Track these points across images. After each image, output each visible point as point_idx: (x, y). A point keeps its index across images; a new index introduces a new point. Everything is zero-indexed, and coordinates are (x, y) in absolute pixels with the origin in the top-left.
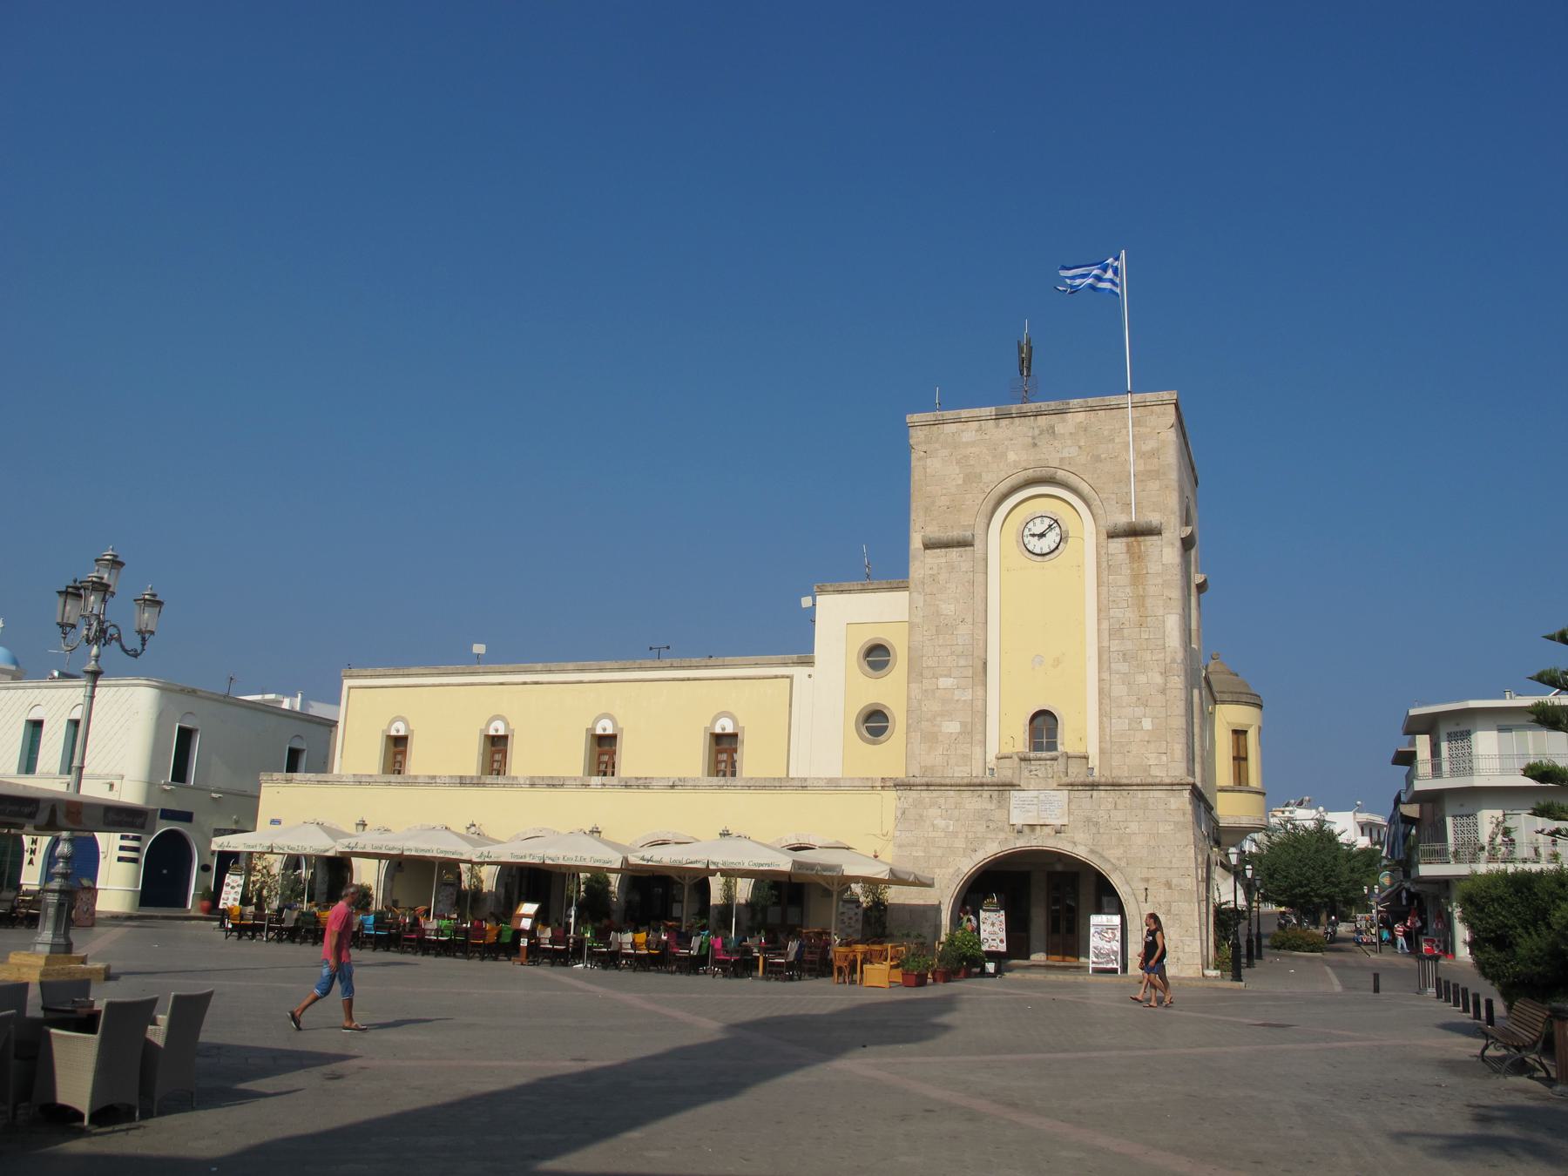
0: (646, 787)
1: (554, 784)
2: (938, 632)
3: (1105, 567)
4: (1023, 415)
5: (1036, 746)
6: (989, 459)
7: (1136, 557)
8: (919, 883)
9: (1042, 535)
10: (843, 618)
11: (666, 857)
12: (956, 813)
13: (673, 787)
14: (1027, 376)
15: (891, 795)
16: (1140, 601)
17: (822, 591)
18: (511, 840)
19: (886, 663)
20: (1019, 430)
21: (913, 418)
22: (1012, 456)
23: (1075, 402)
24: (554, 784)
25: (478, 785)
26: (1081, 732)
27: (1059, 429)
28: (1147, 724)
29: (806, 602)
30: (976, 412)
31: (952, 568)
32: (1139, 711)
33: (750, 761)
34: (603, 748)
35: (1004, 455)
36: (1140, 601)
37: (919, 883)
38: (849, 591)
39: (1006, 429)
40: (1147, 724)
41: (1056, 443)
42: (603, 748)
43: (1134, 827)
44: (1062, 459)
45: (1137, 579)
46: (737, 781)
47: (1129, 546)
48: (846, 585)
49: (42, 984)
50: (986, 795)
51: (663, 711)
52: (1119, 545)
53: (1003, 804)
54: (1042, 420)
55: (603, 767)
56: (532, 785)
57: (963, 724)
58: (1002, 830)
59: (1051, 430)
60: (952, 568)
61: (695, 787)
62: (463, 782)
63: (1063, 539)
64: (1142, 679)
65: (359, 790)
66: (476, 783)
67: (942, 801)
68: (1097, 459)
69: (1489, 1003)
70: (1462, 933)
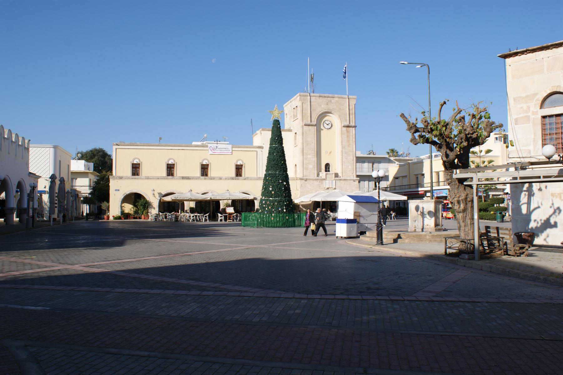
3: (342, 133)
4: (325, 97)
7: (348, 132)
11: (208, 197)
14: (512, 225)
15: (299, 181)
16: (348, 141)
18: (507, 167)
20: (325, 100)
22: (323, 106)
23: (336, 96)
26: (336, 168)
27: (332, 101)
28: (350, 167)
31: (310, 130)
36: (348, 141)
39: (321, 100)
45: (348, 136)
54: (329, 99)
59: (331, 101)
60: (310, 130)
65: (147, 181)
68: (340, 109)
69: (438, 173)
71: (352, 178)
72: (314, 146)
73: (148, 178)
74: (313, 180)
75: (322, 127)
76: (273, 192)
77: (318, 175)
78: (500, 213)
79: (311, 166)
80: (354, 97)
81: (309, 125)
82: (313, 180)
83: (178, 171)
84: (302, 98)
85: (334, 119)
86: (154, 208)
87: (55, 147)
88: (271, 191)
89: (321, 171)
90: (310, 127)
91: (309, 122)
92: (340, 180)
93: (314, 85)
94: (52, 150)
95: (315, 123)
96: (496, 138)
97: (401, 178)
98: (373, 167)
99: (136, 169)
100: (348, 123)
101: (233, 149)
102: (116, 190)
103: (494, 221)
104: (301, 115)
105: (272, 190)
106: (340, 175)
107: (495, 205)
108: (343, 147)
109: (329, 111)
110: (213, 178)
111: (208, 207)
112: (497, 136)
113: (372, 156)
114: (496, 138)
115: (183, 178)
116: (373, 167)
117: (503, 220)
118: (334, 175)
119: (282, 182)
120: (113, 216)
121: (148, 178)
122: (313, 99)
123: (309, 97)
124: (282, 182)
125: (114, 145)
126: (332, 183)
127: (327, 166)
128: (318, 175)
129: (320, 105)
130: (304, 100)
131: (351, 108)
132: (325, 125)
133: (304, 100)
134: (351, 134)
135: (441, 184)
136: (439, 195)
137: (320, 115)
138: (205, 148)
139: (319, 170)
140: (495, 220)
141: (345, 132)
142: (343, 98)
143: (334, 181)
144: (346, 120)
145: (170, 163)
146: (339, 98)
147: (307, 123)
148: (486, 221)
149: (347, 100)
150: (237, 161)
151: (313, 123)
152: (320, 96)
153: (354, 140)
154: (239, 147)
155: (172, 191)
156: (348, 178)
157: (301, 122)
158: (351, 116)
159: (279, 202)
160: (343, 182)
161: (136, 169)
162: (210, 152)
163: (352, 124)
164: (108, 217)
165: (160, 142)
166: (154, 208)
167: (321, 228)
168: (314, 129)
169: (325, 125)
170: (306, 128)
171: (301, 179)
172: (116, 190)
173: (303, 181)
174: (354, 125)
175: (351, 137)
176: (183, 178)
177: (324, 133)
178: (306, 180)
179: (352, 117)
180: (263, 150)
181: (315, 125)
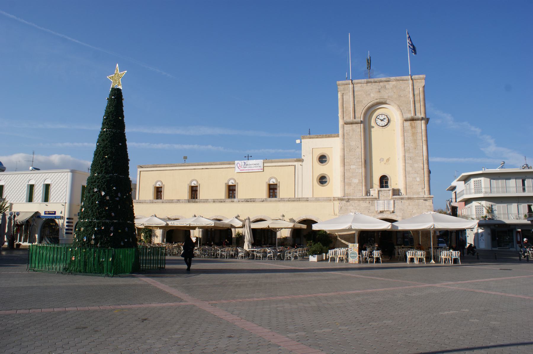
0: (254, 201)
2: (350, 151)
3: (404, 130)
4: (376, 82)
5: (229, 197)
6: (365, 96)
7: (413, 127)
8: (261, 220)
9: (382, 120)
10: (311, 146)
12: (358, 208)
13: (263, 201)
15: (337, 203)
16: (415, 141)
17: (304, 138)
19: (326, 161)
20: (375, 86)
21: (338, 82)
22: (372, 95)
23: (392, 78)
25: (152, 202)
26: (397, 181)
27: (387, 86)
28: (418, 179)
29: (298, 141)
30: (360, 81)
31: (353, 130)
32: (416, 175)
33: (282, 192)
34: (194, 192)
35: (370, 94)
37: (261, 220)
38: (313, 138)
40: (418, 179)
41: (386, 91)
42: (194, 192)
43: (415, 211)
44: (389, 96)
45: (414, 134)
46: (235, 200)
47: (411, 124)
50: (367, 202)
51: (251, 175)
52: (408, 124)
53: (373, 205)
54: (381, 84)
55: (271, 194)
56: (214, 202)
57: (359, 180)
58: (373, 212)
59: (385, 87)
60: (353, 130)
62: (221, 201)
64: (416, 165)
67: (353, 204)
68: (400, 96)
71: (422, 195)
72: (360, 151)
73: (171, 201)
74: (359, 200)
75: (373, 124)
77: (368, 193)
79: (356, 181)
80: (421, 76)
81: (352, 123)
82: (359, 200)
83: (240, 193)
85: (393, 111)
86: (157, 237)
87: (73, 172)
89: (372, 187)
90: (354, 126)
91: (351, 119)
92: (402, 199)
93: (369, 69)
94: (70, 174)
98: (524, 184)
99: (158, 192)
100: (412, 114)
101: (265, 165)
106: (403, 191)
109: (381, 100)
110: (206, 201)
111: (219, 236)
115: (247, 201)
116: (524, 184)
118: (391, 192)
121: (171, 201)
123: (351, 86)
125: (139, 168)
126: (389, 204)
127: (384, 181)
128: (368, 193)
129: (366, 92)
130: (344, 90)
131: (416, 92)
132: (379, 121)
137: (369, 108)
138: (232, 166)
139: (369, 185)
141: (409, 128)
142: (403, 80)
143: (392, 202)
147: (349, 120)
152: (367, 82)
153: (424, 138)
154: (272, 162)
155: (263, 218)
156: (415, 196)
158: (417, 105)
159: (87, 226)
160: (406, 202)
161: (158, 192)
162: (237, 170)
165: (185, 160)
166: (157, 237)
168: (359, 129)
169: (379, 121)
171: (340, 199)
173: (344, 202)
174: (423, 115)
176: (247, 201)
177: (376, 133)
178: (348, 200)
179: (420, 107)
180: (303, 163)
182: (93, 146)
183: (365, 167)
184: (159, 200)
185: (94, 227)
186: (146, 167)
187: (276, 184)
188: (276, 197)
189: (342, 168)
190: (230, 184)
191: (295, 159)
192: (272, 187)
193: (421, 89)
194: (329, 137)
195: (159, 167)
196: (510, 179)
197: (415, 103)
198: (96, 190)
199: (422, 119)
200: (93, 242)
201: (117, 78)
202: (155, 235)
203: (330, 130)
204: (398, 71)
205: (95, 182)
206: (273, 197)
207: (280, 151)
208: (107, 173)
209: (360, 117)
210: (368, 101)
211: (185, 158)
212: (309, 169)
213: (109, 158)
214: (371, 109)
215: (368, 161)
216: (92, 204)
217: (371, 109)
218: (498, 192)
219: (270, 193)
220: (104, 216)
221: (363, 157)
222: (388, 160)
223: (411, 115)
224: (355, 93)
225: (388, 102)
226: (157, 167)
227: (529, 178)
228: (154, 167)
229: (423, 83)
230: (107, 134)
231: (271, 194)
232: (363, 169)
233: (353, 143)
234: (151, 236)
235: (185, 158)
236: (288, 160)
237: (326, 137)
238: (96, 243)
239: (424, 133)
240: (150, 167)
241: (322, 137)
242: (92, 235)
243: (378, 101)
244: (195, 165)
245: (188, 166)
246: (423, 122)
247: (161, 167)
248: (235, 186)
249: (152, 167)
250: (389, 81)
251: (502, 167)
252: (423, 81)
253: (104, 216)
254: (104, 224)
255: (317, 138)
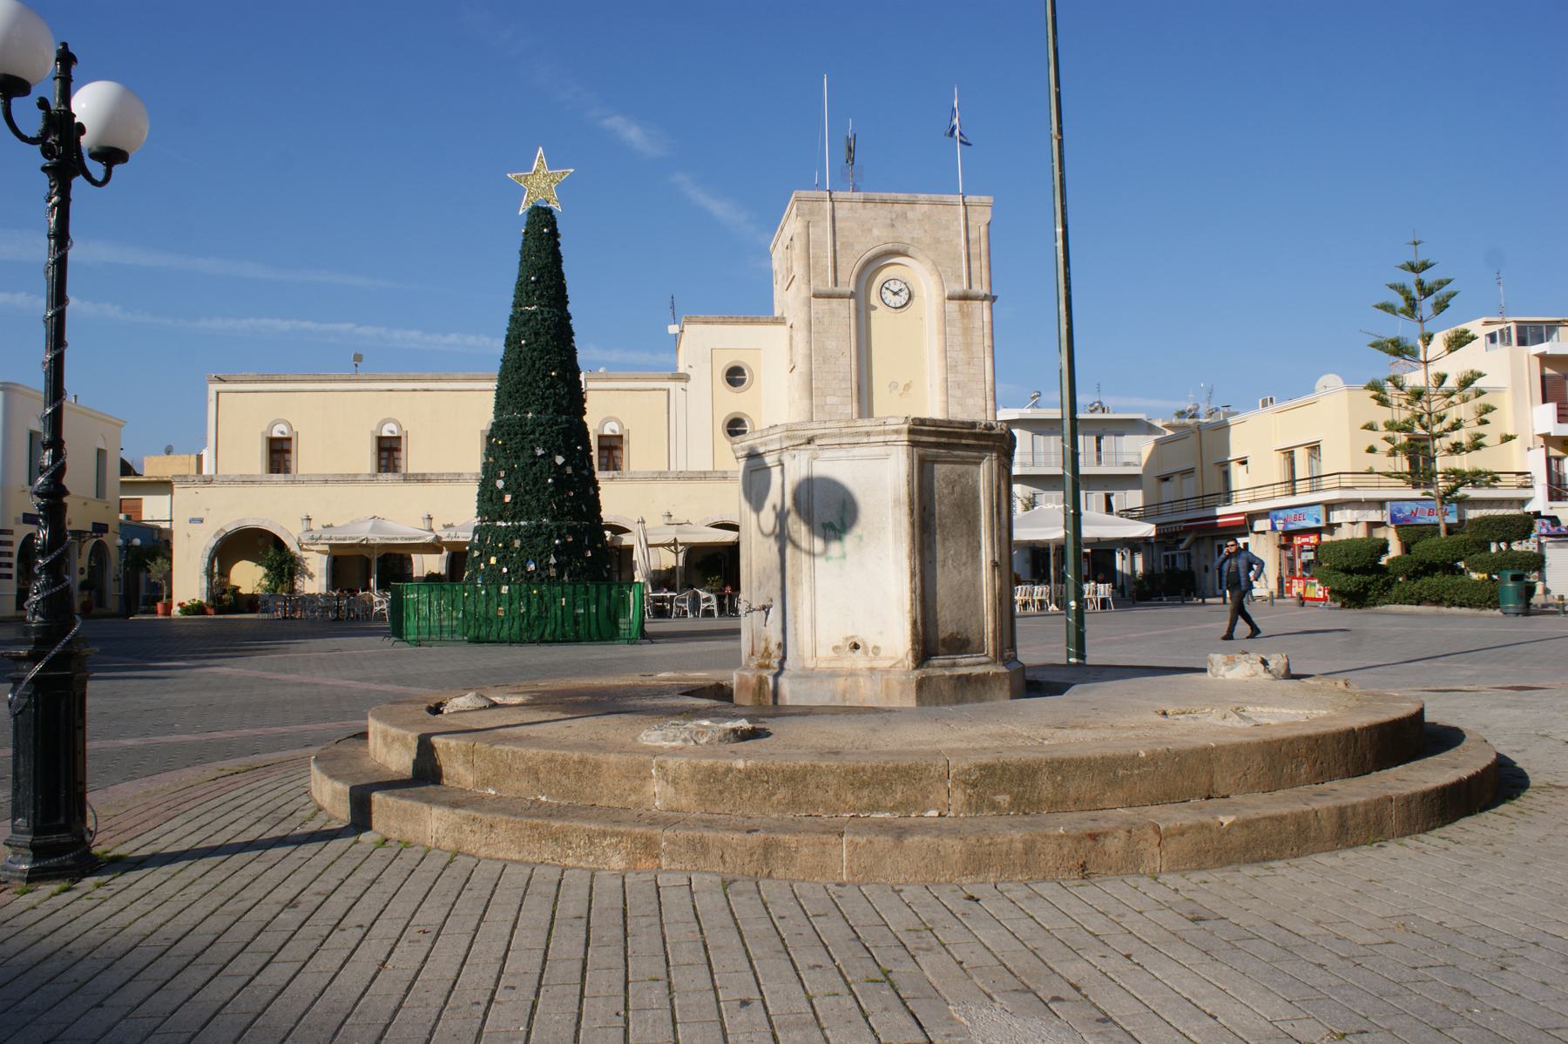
1: (352, 479)
3: (945, 320)
4: (884, 202)
7: (965, 315)
9: (895, 294)
10: (704, 344)
13: (326, 481)
16: (968, 346)
17: (689, 322)
19: (742, 381)
20: (883, 212)
22: (876, 232)
23: (921, 196)
24: (352, 479)
27: (910, 215)
29: (673, 329)
31: (832, 313)
35: (870, 230)
36: (968, 346)
39: (869, 212)
45: (967, 331)
47: (961, 308)
48: (711, 317)
49: (738, 616)
52: (954, 305)
59: (904, 215)
60: (832, 313)
61: (261, 482)
63: (910, 298)
64: (970, 402)
66: (371, 479)
68: (938, 241)
70: (38, 667)
72: (847, 363)
75: (874, 299)
76: (508, 498)
78: (1515, 578)
80: (986, 199)
81: (829, 296)
84: (806, 207)
85: (918, 274)
86: (311, 576)
88: (501, 494)
90: (835, 302)
95: (852, 288)
96: (1492, 337)
97: (1176, 478)
102: (192, 521)
103: (1489, 612)
104: (803, 262)
105: (506, 489)
107: (1494, 548)
108: (949, 368)
109: (897, 247)
112: (1495, 328)
113: (1098, 416)
114: (1492, 337)
117: (1528, 605)
119: (549, 456)
120: (180, 605)
122: (842, 211)
123: (828, 205)
124: (549, 456)
125: (212, 381)
129: (866, 223)
130: (811, 213)
132: (888, 295)
133: (811, 213)
134: (978, 324)
135: (1300, 486)
136: (1291, 527)
137: (869, 262)
140: (1496, 605)
141: (956, 315)
142: (945, 204)
144: (960, 277)
145: (385, 433)
146: (933, 203)
147: (823, 289)
148: (1455, 610)
149: (961, 209)
150: (603, 425)
151: (841, 289)
152: (866, 201)
153: (987, 342)
157: (804, 288)
158: (975, 265)
159: (529, 536)
163: (980, 288)
164: (168, 609)
165: (358, 365)
166: (311, 576)
167: (1240, 620)
169: (888, 295)
170: (819, 305)
172: (192, 521)
174: (985, 290)
175: (978, 333)
179: (980, 267)
180: (689, 386)
181: (852, 295)
182: (498, 347)
183: (859, 401)
184: (281, 477)
185: (550, 536)
186: (235, 382)
187: (621, 437)
188: (287, 471)
189: (806, 402)
190: (276, 434)
191: (669, 374)
192: (387, 444)
193: (983, 229)
194: (752, 322)
195: (280, 381)
196: (1122, 434)
197: (969, 261)
198: (540, 452)
199: (985, 298)
200: (553, 572)
201: (540, 182)
202: (304, 572)
203: (754, 306)
204: (938, 182)
205: (533, 432)
206: (386, 471)
207: (308, 324)
208: (558, 412)
209: (848, 284)
210: (866, 247)
211: (358, 358)
212: (706, 403)
213: (558, 376)
214: (872, 266)
215: (864, 388)
216: (535, 483)
217: (872, 266)
218: (1048, 465)
219: (380, 458)
220: (569, 513)
221: (854, 379)
222: (907, 386)
223: (961, 287)
224: (838, 225)
225: (911, 251)
226: (272, 381)
227: (1110, 433)
228: (262, 381)
229: (986, 215)
230: (544, 320)
231: (384, 462)
232: (855, 405)
233: (831, 344)
234: (292, 574)
235: (358, 358)
236: (651, 374)
237: (745, 323)
238: (560, 575)
239: (987, 330)
240: (250, 381)
241: (737, 323)
242: (548, 556)
243: (889, 247)
244: (392, 380)
245: (370, 381)
246: (986, 303)
247: (285, 381)
248: (289, 439)
249: (256, 381)
250: (913, 203)
251: (1035, 405)
252: (988, 210)
253: (569, 513)
254: (572, 531)
255: (723, 323)
